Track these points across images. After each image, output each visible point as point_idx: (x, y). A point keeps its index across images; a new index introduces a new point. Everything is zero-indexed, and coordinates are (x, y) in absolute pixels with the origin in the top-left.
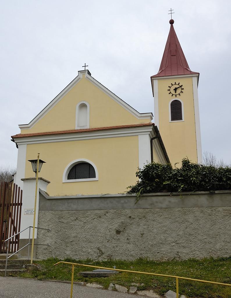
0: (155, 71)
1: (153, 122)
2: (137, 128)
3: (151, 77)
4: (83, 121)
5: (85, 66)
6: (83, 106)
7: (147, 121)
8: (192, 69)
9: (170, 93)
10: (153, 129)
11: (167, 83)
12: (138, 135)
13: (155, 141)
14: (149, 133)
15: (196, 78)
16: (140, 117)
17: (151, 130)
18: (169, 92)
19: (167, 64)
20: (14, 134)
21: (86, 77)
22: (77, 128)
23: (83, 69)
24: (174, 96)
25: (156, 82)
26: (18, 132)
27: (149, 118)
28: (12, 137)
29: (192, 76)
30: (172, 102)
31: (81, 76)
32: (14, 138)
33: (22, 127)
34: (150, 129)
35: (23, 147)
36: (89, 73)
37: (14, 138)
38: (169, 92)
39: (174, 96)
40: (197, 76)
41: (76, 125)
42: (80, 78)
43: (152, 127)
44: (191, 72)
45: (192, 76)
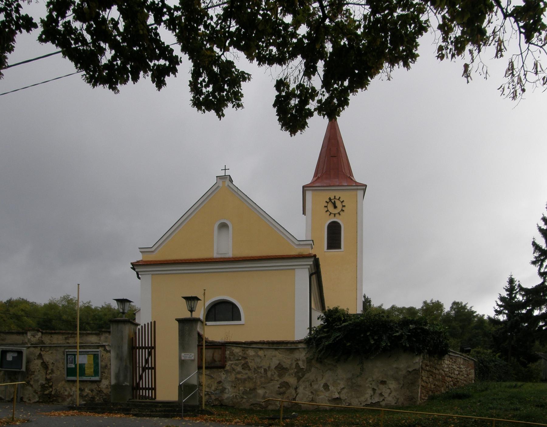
0: (309, 178)
1: (313, 252)
2: (305, 260)
3: (303, 187)
4: (224, 246)
5: (225, 169)
6: (223, 226)
7: (307, 251)
8: (358, 177)
9: (331, 213)
10: (313, 262)
11: (325, 196)
12: (294, 269)
13: (314, 277)
14: (309, 267)
15: (362, 192)
16: (299, 245)
17: (312, 263)
18: (328, 213)
19: (325, 168)
20: (134, 261)
21: (226, 185)
22: (215, 255)
23: (222, 173)
24: (332, 215)
25: (309, 194)
26: (139, 257)
27: (310, 247)
28: (132, 264)
29: (357, 189)
30: (330, 223)
31: (220, 183)
32: (134, 266)
33: (143, 251)
34: (311, 262)
35: (147, 279)
36: (231, 181)
37: (134, 266)
38: (328, 213)
39: (332, 215)
40: (363, 189)
41: (215, 252)
42: (218, 186)
43: (312, 259)
44: (356, 182)
45: (357, 189)
